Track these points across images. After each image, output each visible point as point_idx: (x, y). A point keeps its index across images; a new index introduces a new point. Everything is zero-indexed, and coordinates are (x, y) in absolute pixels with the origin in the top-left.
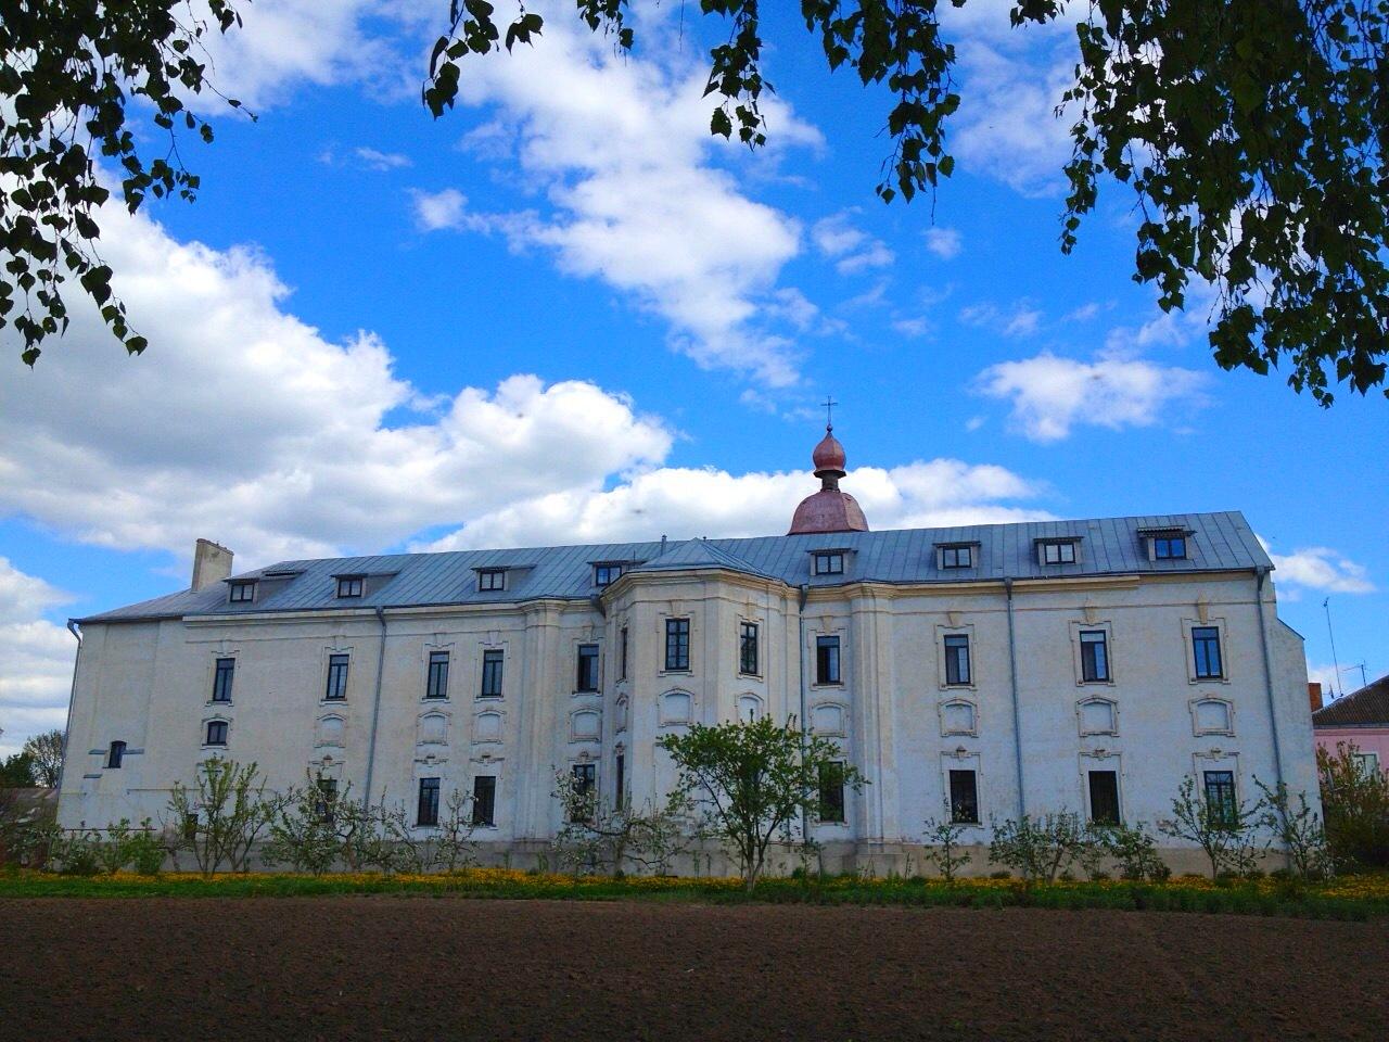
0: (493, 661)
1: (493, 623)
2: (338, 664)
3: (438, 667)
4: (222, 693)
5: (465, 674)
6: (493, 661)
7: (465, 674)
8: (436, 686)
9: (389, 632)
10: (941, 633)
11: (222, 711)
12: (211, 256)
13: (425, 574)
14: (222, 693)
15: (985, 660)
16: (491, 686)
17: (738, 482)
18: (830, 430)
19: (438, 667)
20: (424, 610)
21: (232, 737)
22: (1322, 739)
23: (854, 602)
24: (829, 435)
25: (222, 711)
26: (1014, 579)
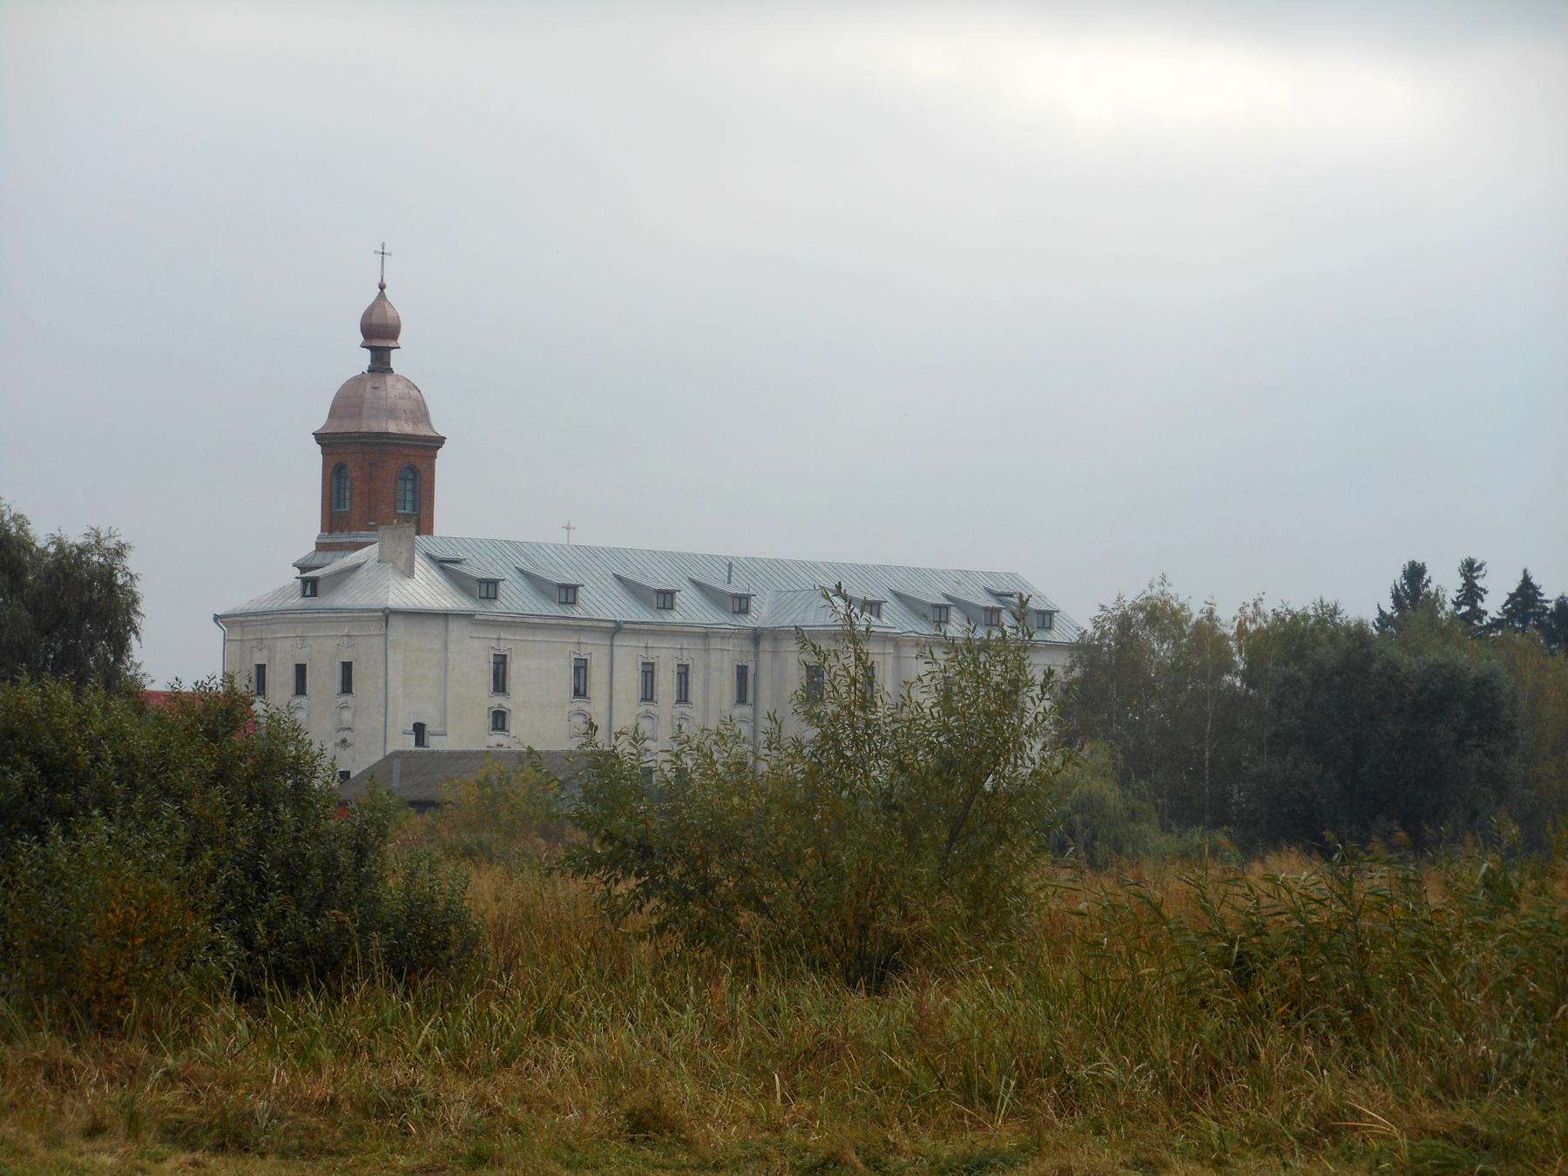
0: (683, 673)
1: (686, 643)
2: (581, 669)
3: (649, 672)
4: (500, 683)
5: (666, 683)
6: (683, 673)
7: (666, 683)
8: (648, 695)
9: (761, 649)
10: (641, 660)
11: (498, 701)
12: (390, 322)
13: (424, 578)
14: (500, 683)
15: (597, 676)
16: (683, 697)
17: (1132, 590)
18: (382, 287)
19: (649, 672)
20: (645, 627)
21: (513, 724)
22: (1554, 602)
23: (712, 640)
24: (382, 296)
25: (498, 701)
26: (625, 622)
